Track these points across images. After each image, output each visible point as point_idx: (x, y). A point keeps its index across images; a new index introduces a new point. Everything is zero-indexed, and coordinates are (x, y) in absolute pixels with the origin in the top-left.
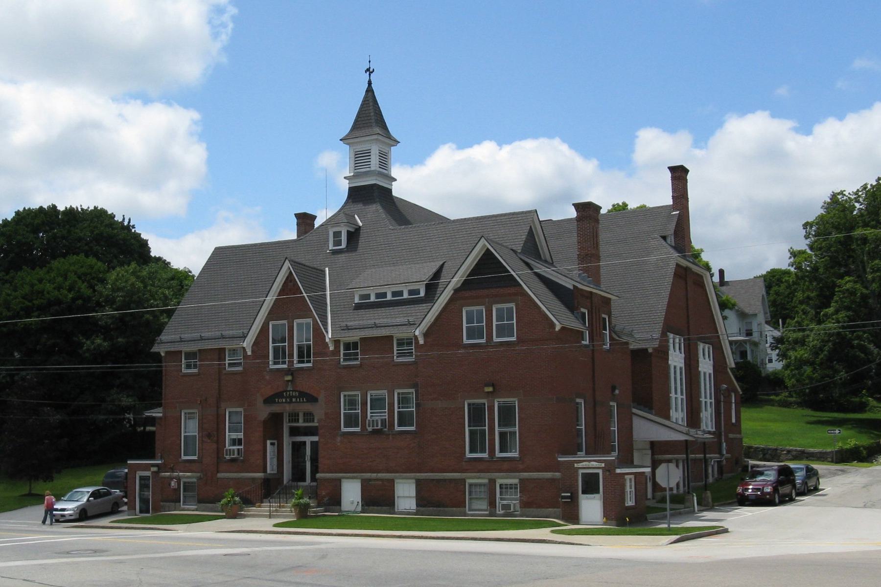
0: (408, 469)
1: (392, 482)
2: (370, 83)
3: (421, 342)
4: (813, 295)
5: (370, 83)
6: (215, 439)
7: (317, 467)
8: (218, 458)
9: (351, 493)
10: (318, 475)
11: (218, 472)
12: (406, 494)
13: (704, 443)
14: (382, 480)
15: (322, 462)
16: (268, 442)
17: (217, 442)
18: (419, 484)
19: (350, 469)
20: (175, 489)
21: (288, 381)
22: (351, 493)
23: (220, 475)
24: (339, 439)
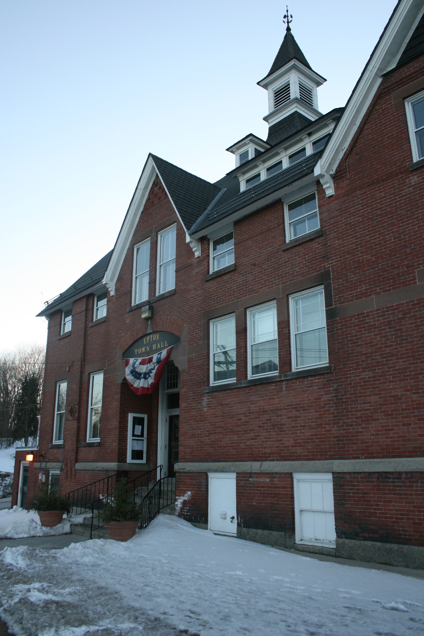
0: (315, 453)
1: (288, 477)
2: (288, 29)
3: (330, 192)
4: (288, 534)
5: (288, 29)
6: (76, 415)
7: (177, 453)
8: (78, 441)
9: (223, 493)
10: (177, 466)
11: (77, 461)
12: (314, 501)
13: (91, 539)
14: (271, 475)
15: (185, 442)
16: (131, 416)
17: (79, 420)
18: (340, 482)
19: (221, 457)
20: (43, 483)
21: (147, 319)
22: (223, 493)
23: (78, 466)
24: (205, 400)
